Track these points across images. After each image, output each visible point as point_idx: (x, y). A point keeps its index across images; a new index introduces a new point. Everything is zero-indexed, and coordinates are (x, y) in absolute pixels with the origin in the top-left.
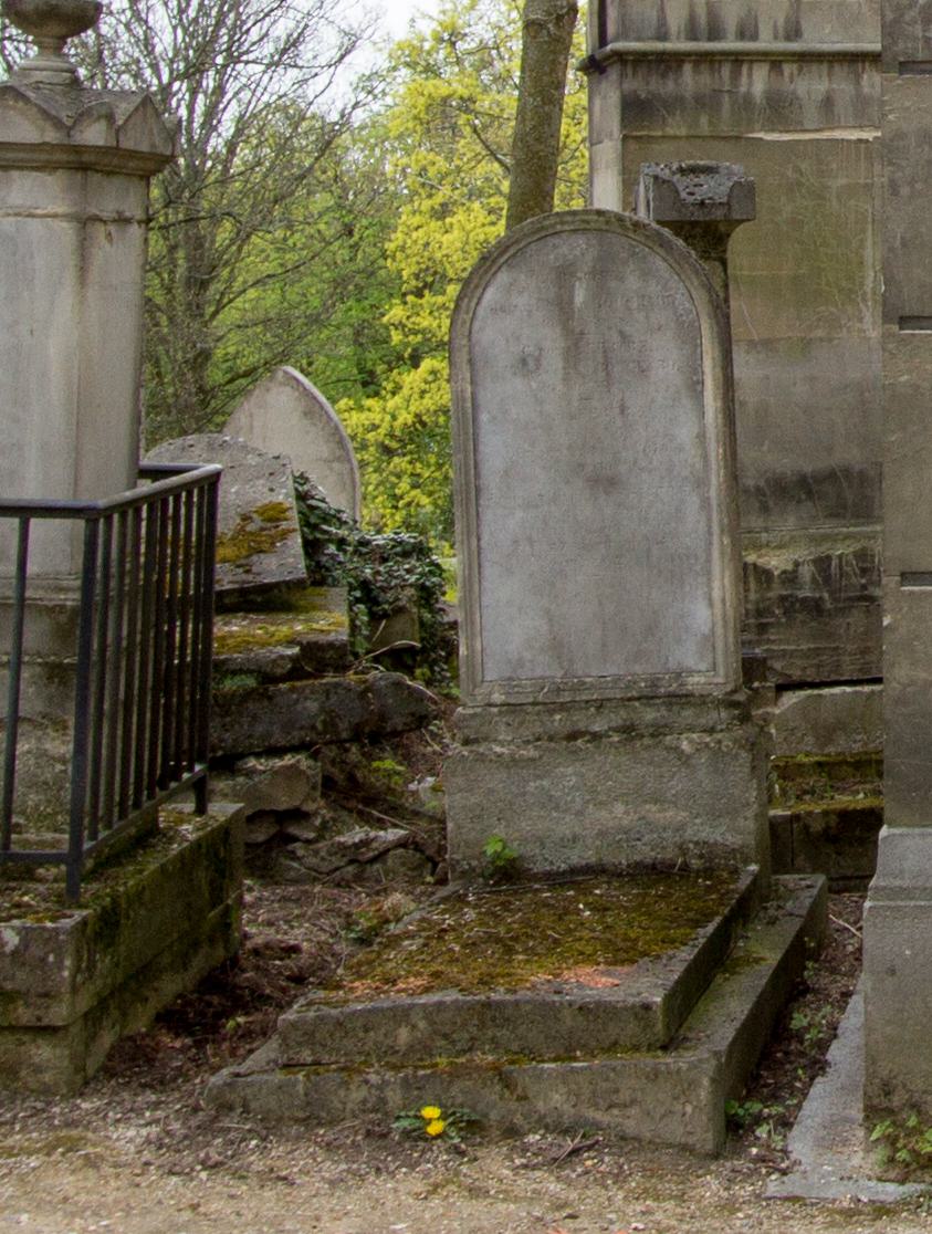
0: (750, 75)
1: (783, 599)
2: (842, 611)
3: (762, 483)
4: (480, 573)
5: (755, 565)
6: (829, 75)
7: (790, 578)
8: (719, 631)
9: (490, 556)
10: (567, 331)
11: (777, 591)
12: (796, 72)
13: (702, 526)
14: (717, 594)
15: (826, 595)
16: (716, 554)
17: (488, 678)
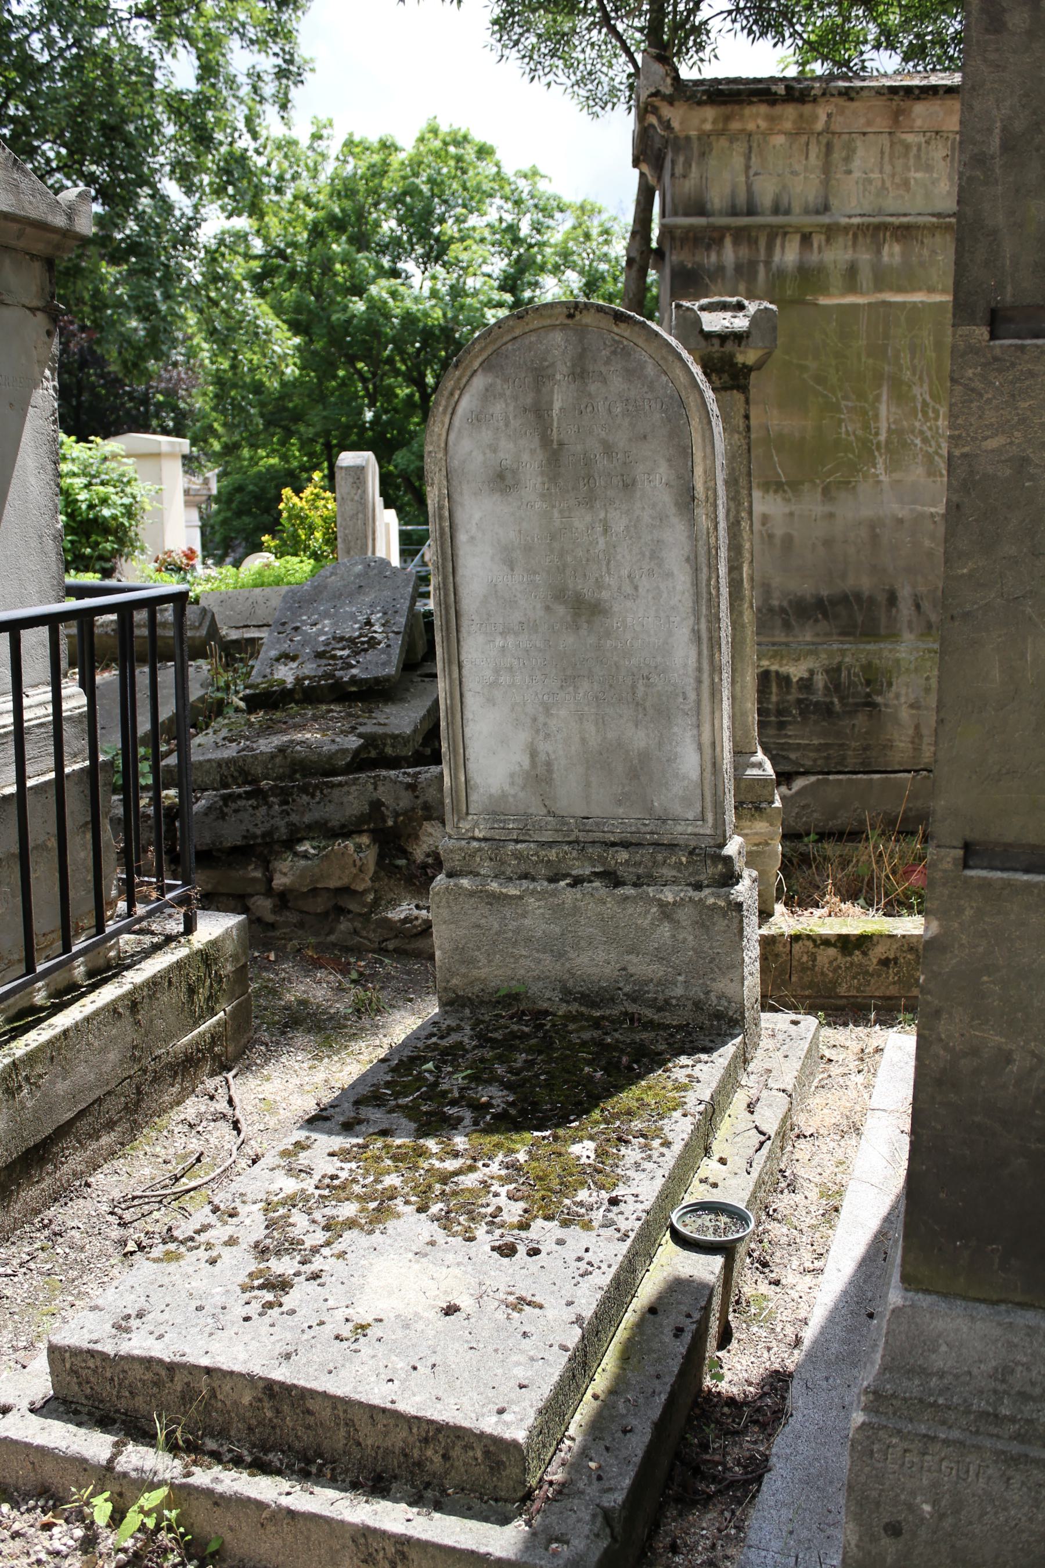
0: (783, 247)
1: (799, 701)
2: (852, 713)
3: (785, 604)
5: (777, 672)
6: (854, 245)
7: (806, 684)
10: (545, 441)
11: (794, 695)
12: (823, 243)
13: (692, 661)
15: (836, 700)
17: (471, 811)
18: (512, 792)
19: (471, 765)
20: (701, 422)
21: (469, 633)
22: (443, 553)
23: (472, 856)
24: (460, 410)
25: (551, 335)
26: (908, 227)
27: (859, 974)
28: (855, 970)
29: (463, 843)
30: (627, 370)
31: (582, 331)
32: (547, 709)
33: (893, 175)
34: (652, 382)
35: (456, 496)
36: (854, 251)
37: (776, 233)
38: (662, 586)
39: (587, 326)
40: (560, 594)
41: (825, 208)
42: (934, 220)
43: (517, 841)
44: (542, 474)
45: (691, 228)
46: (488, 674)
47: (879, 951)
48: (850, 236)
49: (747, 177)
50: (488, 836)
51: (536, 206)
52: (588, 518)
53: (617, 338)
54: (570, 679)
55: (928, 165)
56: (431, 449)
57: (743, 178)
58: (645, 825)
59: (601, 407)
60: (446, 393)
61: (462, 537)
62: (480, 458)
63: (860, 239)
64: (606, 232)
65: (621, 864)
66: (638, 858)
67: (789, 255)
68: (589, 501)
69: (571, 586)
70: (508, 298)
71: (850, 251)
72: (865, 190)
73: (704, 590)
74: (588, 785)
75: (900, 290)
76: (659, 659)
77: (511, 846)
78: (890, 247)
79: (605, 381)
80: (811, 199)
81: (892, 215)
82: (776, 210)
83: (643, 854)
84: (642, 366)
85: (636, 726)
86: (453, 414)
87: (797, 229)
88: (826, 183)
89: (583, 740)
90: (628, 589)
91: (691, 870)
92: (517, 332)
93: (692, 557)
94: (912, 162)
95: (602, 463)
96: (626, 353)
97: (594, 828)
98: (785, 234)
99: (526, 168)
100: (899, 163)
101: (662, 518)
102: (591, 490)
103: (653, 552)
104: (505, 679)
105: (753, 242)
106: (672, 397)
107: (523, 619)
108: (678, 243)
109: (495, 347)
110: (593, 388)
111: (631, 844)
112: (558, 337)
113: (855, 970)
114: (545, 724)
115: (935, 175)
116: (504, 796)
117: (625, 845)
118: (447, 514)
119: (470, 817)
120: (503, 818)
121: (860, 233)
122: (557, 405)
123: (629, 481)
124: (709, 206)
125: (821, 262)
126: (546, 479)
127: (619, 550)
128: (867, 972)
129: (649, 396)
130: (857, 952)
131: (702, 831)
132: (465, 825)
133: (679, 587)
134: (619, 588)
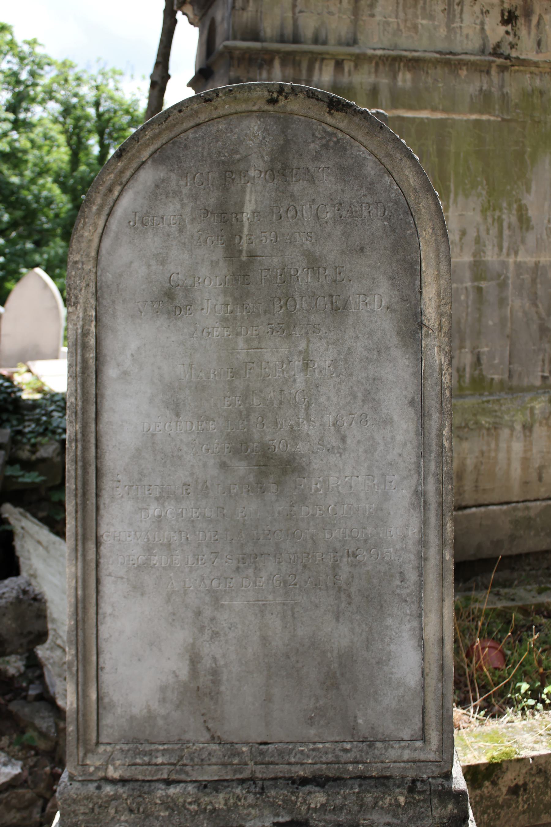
0: (321, 70)
4: (98, 592)
6: (376, 71)
8: (432, 681)
9: (113, 565)
10: (231, 251)
12: (352, 68)
13: (413, 532)
14: (431, 632)
16: (432, 576)
17: (103, 739)
18: (163, 712)
19: (107, 677)
20: (434, 233)
21: (113, 498)
22: (85, 393)
23: (104, 806)
24: (119, 211)
25: (245, 123)
26: (417, 60)
27: (488, 807)
28: (485, 803)
29: (92, 787)
30: (341, 168)
31: (285, 121)
32: (216, 598)
33: (406, 21)
34: (372, 183)
35: (106, 320)
36: (376, 76)
37: (316, 59)
38: (378, 438)
39: (292, 113)
40: (240, 447)
41: (354, 42)
42: (438, 56)
43: (168, 782)
44: (225, 292)
45: (248, 50)
46: (137, 554)
47: (508, 779)
48: (373, 64)
49: (294, 13)
50: (127, 775)
51: (33, 61)
52: (284, 350)
53: (329, 129)
54: (250, 558)
55: (431, 15)
56: (77, 258)
57: (290, 14)
58: (346, 751)
59: (307, 212)
60: (103, 189)
61: (111, 372)
62: (143, 271)
63: (381, 67)
64: (78, 79)
65: (315, 810)
66: (339, 800)
67: (325, 76)
68: (287, 328)
69: (256, 436)
70: (11, 116)
71: (373, 76)
72: (384, 30)
73: (434, 442)
74: (268, 699)
75: (411, 108)
76: (370, 530)
77: (161, 792)
78: (404, 74)
79: (312, 180)
80: (343, 33)
81: (406, 50)
82: (316, 41)
83: (347, 795)
84: (360, 164)
85: (337, 619)
86: (109, 215)
87: (333, 57)
88: (355, 22)
89: (265, 640)
90: (333, 440)
91: (411, 813)
92: (203, 117)
93: (418, 399)
94: (419, 12)
95: (305, 280)
96: (340, 148)
97: (276, 759)
98: (323, 59)
99: (30, 38)
100: (410, 11)
101: (380, 350)
102: (289, 314)
103: (367, 392)
104: (159, 559)
105: (297, 65)
106: (396, 203)
107: (189, 480)
108: (236, 62)
109: (172, 135)
110: (296, 188)
111: (328, 779)
112: (254, 126)
113: (485, 803)
114: (212, 619)
115: (436, 23)
116: (151, 717)
117: (319, 781)
118: (92, 342)
119: (101, 749)
120: (148, 747)
121: (380, 62)
122: (249, 208)
123: (339, 304)
124: (262, 34)
125: (351, 83)
126: (230, 299)
127: (322, 389)
128: (496, 805)
129: (369, 199)
130: (487, 783)
131: (422, 757)
132: (93, 762)
133: (399, 438)
134: (321, 439)
